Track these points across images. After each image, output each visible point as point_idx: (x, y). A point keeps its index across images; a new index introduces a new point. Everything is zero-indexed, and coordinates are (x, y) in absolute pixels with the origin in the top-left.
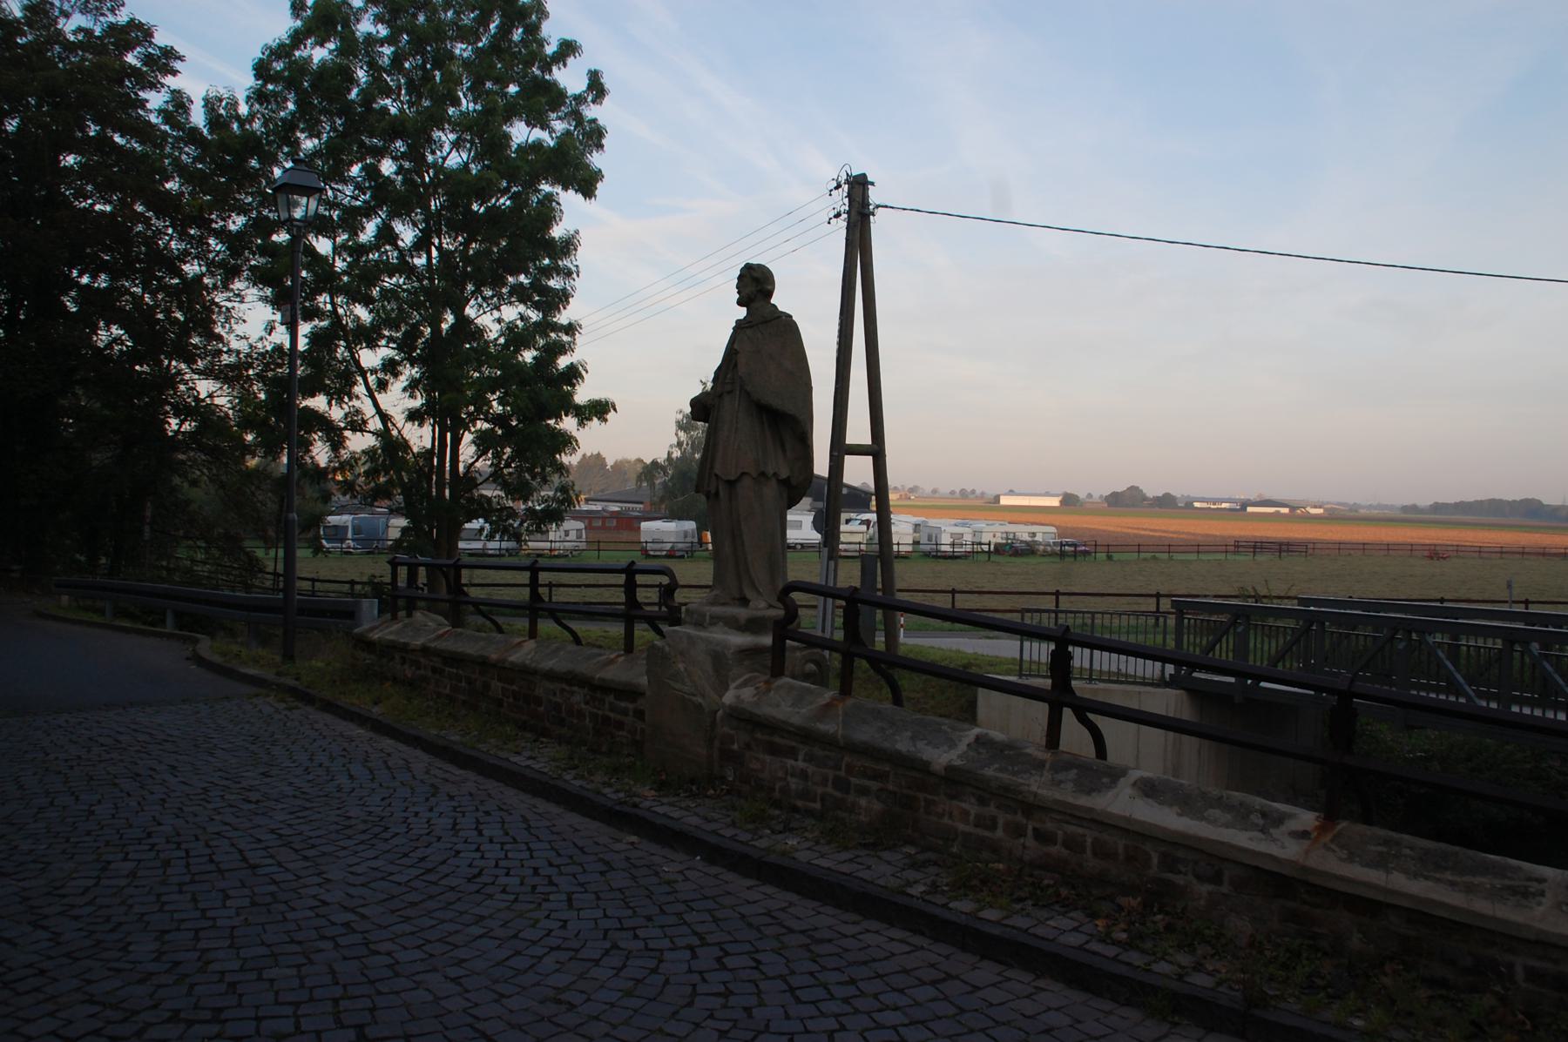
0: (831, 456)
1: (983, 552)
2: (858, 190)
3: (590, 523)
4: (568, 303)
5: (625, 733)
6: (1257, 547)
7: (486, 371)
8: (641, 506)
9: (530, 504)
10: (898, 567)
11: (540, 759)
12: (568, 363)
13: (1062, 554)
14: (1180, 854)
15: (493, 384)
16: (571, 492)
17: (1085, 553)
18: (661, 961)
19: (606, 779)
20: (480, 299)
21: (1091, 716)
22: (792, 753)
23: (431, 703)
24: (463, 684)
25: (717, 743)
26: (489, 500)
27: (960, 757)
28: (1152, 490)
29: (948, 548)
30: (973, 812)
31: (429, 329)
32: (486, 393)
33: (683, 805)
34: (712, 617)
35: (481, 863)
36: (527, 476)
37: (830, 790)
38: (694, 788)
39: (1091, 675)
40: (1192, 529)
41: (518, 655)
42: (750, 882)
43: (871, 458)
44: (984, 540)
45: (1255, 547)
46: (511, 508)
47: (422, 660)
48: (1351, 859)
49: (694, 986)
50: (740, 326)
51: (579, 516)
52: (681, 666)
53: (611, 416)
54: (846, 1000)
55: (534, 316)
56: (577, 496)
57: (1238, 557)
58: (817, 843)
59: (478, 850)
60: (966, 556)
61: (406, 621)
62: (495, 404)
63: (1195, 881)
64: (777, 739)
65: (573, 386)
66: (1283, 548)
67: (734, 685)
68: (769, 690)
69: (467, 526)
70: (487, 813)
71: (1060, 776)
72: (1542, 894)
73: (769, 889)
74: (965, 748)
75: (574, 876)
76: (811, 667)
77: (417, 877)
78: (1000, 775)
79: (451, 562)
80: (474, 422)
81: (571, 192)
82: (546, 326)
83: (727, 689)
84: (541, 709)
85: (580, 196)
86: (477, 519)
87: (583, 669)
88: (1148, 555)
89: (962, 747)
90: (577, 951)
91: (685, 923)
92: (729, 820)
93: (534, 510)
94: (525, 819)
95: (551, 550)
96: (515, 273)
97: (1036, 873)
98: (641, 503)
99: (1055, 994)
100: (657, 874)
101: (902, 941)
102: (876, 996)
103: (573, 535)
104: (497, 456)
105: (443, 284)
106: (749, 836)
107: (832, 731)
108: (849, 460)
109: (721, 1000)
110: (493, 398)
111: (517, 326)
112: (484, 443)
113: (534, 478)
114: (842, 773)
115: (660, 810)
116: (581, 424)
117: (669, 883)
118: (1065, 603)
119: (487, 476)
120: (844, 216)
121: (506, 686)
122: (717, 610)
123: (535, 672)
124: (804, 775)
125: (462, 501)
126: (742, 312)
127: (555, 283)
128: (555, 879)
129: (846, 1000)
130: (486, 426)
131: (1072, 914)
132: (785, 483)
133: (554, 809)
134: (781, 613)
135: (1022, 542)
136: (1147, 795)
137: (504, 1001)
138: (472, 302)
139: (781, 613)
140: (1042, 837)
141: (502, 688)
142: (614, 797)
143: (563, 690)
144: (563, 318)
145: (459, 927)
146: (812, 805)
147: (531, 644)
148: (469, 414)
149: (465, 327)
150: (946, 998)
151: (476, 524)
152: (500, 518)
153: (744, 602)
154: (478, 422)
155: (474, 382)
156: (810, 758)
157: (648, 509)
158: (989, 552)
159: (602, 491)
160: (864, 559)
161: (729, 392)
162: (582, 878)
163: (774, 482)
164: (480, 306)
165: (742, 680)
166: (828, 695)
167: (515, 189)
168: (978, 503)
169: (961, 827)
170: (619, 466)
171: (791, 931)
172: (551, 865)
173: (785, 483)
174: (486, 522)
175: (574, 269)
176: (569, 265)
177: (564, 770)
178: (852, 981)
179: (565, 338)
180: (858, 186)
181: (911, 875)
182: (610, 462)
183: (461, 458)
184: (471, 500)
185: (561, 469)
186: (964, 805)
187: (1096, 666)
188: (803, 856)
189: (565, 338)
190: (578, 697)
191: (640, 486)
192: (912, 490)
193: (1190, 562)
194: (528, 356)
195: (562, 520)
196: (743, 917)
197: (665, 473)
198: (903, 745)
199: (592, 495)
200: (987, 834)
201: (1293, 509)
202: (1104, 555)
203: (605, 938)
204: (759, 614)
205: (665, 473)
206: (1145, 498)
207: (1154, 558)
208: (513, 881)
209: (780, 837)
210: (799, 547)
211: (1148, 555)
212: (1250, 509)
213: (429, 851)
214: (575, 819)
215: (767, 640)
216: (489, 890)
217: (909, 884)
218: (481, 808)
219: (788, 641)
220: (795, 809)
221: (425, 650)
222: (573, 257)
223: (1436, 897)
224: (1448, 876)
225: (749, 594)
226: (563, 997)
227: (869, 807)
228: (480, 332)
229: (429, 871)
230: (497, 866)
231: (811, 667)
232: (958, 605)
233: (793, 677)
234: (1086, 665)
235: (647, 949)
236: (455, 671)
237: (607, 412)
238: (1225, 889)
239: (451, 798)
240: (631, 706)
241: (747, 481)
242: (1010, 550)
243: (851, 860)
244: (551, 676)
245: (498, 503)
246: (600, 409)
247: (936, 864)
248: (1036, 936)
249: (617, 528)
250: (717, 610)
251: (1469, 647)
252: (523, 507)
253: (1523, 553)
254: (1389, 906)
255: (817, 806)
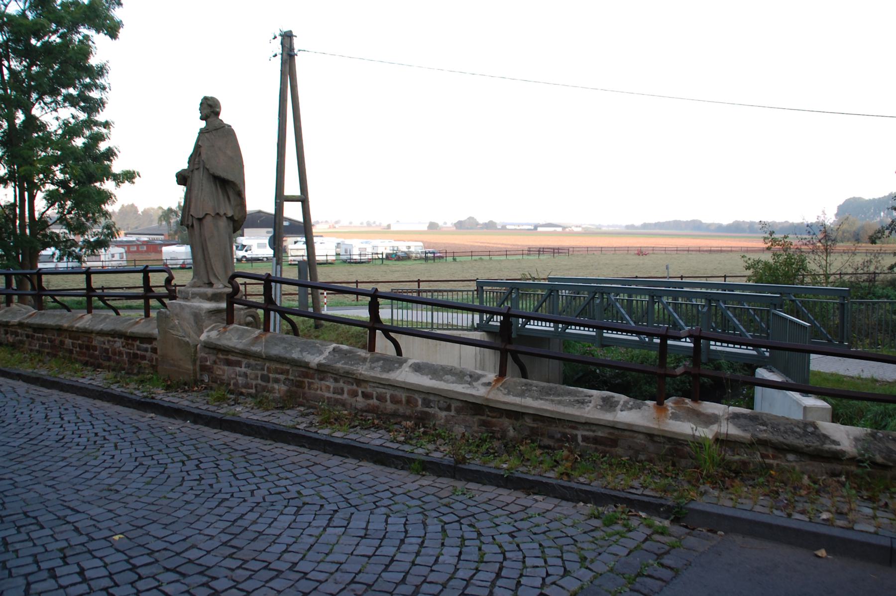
0: (276, 203)
1: (379, 259)
2: (287, 40)
3: (129, 248)
4: (104, 107)
5: (146, 362)
6: (541, 251)
7: (50, 151)
8: (162, 237)
9: (86, 237)
10: (320, 270)
11: (98, 379)
12: (107, 147)
13: (426, 259)
14: (432, 398)
15: (56, 161)
16: (113, 229)
17: (442, 257)
18: (166, 468)
19: (136, 386)
20: (42, 104)
21: (392, 334)
22: (239, 364)
23: (27, 355)
24: (47, 343)
25: (198, 363)
26: (58, 235)
27: (324, 359)
28: (482, 219)
29: (357, 257)
30: (332, 386)
31: (6, 124)
32: (51, 166)
33: (180, 396)
34: (193, 294)
35: (64, 433)
36: (83, 219)
37: (259, 382)
38: (186, 387)
39: (432, 326)
40: (504, 242)
41: (81, 323)
42: (215, 431)
43: (300, 203)
44: (380, 252)
45: (539, 251)
46: (73, 240)
47: (19, 331)
48: (508, 394)
49: (183, 478)
50: (202, 132)
51: (120, 244)
52: (176, 322)
53: (137, 180)
54: (262, 477)
55: (83, 116)
56: (118, 231)
57: (530, 257)
58: (252, 409)
59: (61, 427)
60: (369, 261)
61: (7, 308)
62: (58, 173)
63: (438, 410)
64: (230, 357)
65: (111, 161)
66: (555, 251)
67: (207, 330)
68: (225, 332)
69: (43, 252)
70: (66, 409)
71: (373, 365)
72: (590, 402)
73: (226, 433)
74: (327, 354)
75: (118, 435)
76: (250, 319)
77: (25, 443)
78: (345, 366)
79: (35, 271)
80: (44, 184)
81: (102, 34)
82: (89, 123)
83: (202, 332)
84: (97, 353)
85: (108, 37)
86: (50, 247)
87: (120, 327)
88: (477, 258)
89: (326, 354)
90: (120, 468)
91: (180, 451)
92: (205, 401)
93: (89, 241)
94: (89, 410)
95: (103, 267)
96: (66, 86)
97: (364, 414)
98: (162, 235)
99: (368, 468)
100: (165, 430)
101: (293, 451)
102: (277, 475)
103: (117, 257)
104: (62, 206)
105: (14, 93)
106: (216, 408)
107: (259, 350)
108: (286, 205)
109: (198, 482)
110: (56, 169)
111: (70, 123)
112: (52, 198)
113: (88, 220)
114: (265, 372)
115: (167, 399)
116: (118, 185)
117: (171, 434)
118: (424, 286)
119: (55, 220)
120: (279, 57)
121: (75, 341)
122: (196, 290)
123: (92, 332)
124: (245, 375)
125: (38, 236)
126: (203, 124)
127: (95, 94)
128: (107, 437)
129: (262, 477)
130: (52, 187)
131: (380, 431)
132: (231, 219)
133: (106, 405)
134: (231, 290)
135: (402, 252)
136: (416, 371)
137: (79, 492)
138: (37, 106)
139: (231, 290)
140: (366, 396)
141: (72, 343)
142: (141, 395)
143: (109, 341)
144: (100, 117)
145: (51, 463)
146: (251, 391)
147: (89, 316)
148: (41, 180)
149: (32, 122)
150: (313, 473)
151: (49, 251)
152: (66, 246)
153: (210, 284)
154: (47, 185)
155: (42, 159)
156: (248, 366)
157: (167, 238)
158: (382, 259)
159: (136, 228)
160: (300, 264)
161: (197, 169)
162: (122, 436)
163: (224, 218)
164: (43, 108)
165: (209, 328)
166: (257, 332)
167: (61, 31)
168: (378, 229)
169: (327, 394)
170: (146, 212)
171: (236, 450)
172: (104, 430)
173: (231, 219)
174: (57, 248)
175: (107, 86)
176: (104, 83)
177: (112, 384)
178: (266, 469)
179: (103, 131)
180: (287, 38)
181: (300, 420)
182: (140, 210)
183: (36, 208)
184: (45, 236)
185: (106, 214)
186: (328, 383)
187: (435, 321)
188: (244, 415)
189: (103, 131)
190: (119, 344)
191: (161, 224)
192: (337, 222)
193: (501, 261)
194: (79, 142)
195: (108, 246)
196: (211, 446)
197: (177, 215)
198: (295, 355)
199: (130, 231)
200: (339, 397)
201: (564, 228)
202: (451, 258)
203: (136, 461)
204: (219, 291)
205: (177, 215)
206: (478, 224)
207: (481, 259)
208: (83, 440)
209: (232, 407)
210: (265, 259)
211: (477, 258)
212: (539, 229)
213: (31, 430)
214: (119, 408)
215: (224, 305)
216: (69, 445)
217: (298, 424)
218: (62, 407)
219: (235, 305)
220: (242, 394)
221: (21, 325)
222: (106, 78)
223: (545, 407)
224: (552, 397)
225: (213, 280)
226: (112, 488)
227: (280, 389)
228: (43, 127)
229: (31, 439)
230: (73, 433)
231: (250, 319)
232: (359, 287)
233: (240, 324)
234: (430, 320)
235: (158, 463)
236: (41, 335)
237: (134, 178)
238: (453, 413)
239: (43, 404)
240: (149, 346)
241: (209, 218)
242: (395, 257)
243: (269, 415)
244: (101, 333)
245: (64, 237)
246: (129, 176)
247: (313, 414)
248: (360, 442)
249: (147, 251)
250: (196, 290)
251: (637, 301)
252: (82, 239)
253: (688, 251)
254: (523, 414)
255: (253, 391)
